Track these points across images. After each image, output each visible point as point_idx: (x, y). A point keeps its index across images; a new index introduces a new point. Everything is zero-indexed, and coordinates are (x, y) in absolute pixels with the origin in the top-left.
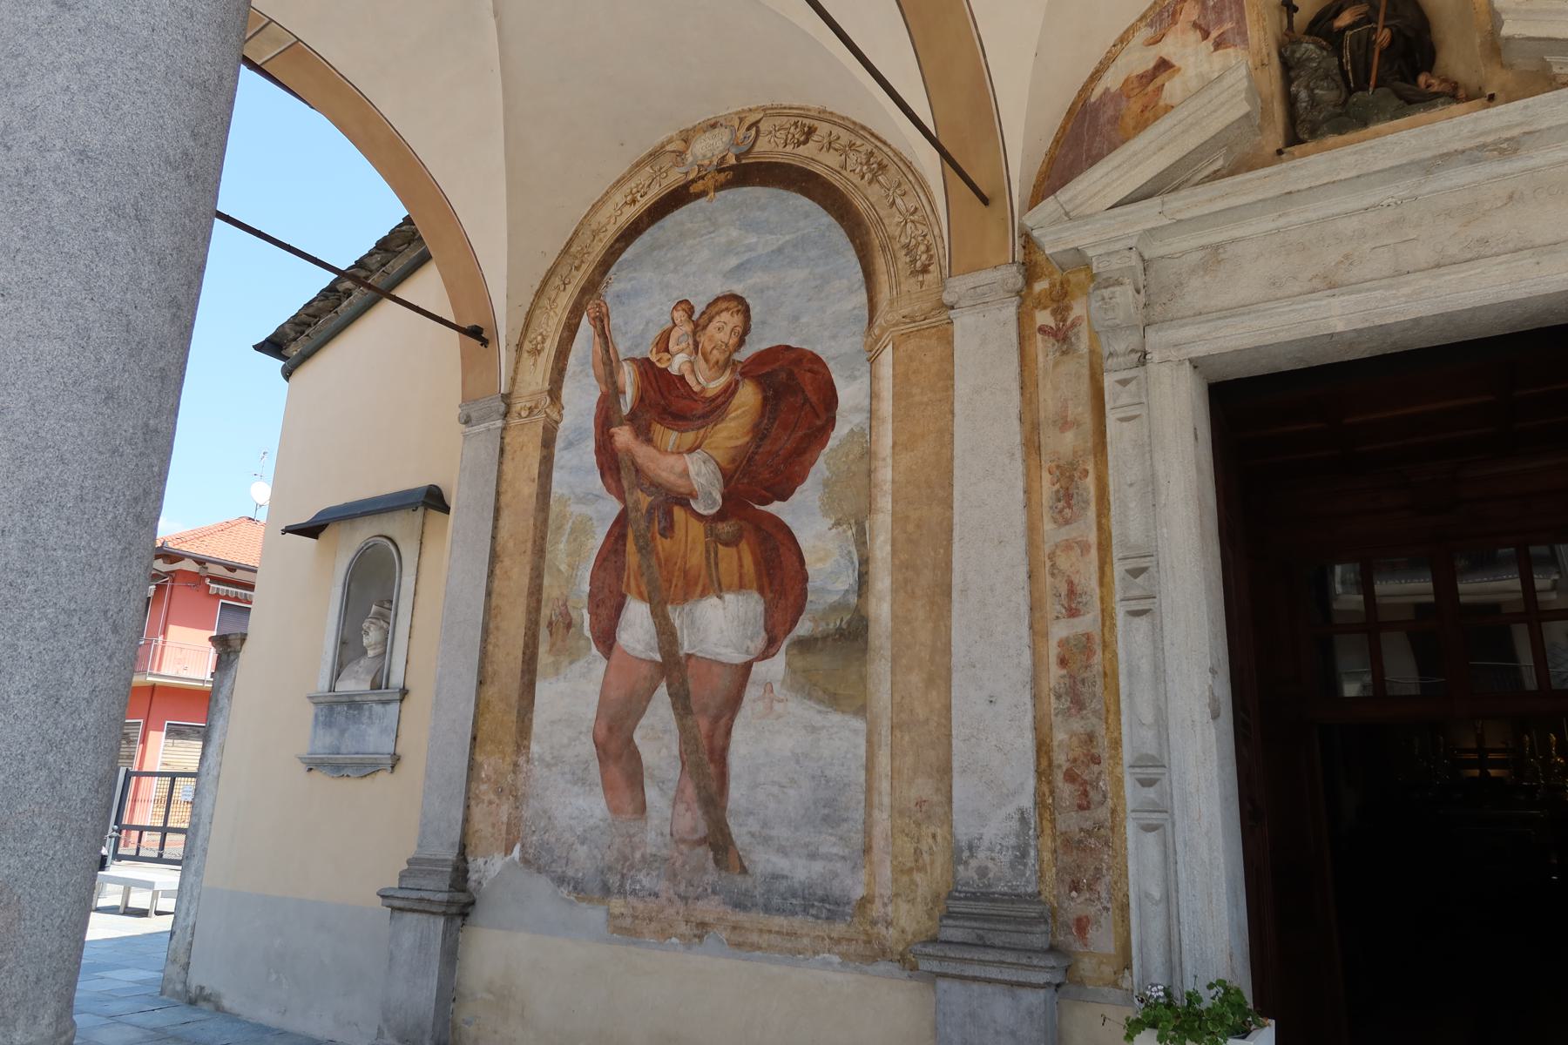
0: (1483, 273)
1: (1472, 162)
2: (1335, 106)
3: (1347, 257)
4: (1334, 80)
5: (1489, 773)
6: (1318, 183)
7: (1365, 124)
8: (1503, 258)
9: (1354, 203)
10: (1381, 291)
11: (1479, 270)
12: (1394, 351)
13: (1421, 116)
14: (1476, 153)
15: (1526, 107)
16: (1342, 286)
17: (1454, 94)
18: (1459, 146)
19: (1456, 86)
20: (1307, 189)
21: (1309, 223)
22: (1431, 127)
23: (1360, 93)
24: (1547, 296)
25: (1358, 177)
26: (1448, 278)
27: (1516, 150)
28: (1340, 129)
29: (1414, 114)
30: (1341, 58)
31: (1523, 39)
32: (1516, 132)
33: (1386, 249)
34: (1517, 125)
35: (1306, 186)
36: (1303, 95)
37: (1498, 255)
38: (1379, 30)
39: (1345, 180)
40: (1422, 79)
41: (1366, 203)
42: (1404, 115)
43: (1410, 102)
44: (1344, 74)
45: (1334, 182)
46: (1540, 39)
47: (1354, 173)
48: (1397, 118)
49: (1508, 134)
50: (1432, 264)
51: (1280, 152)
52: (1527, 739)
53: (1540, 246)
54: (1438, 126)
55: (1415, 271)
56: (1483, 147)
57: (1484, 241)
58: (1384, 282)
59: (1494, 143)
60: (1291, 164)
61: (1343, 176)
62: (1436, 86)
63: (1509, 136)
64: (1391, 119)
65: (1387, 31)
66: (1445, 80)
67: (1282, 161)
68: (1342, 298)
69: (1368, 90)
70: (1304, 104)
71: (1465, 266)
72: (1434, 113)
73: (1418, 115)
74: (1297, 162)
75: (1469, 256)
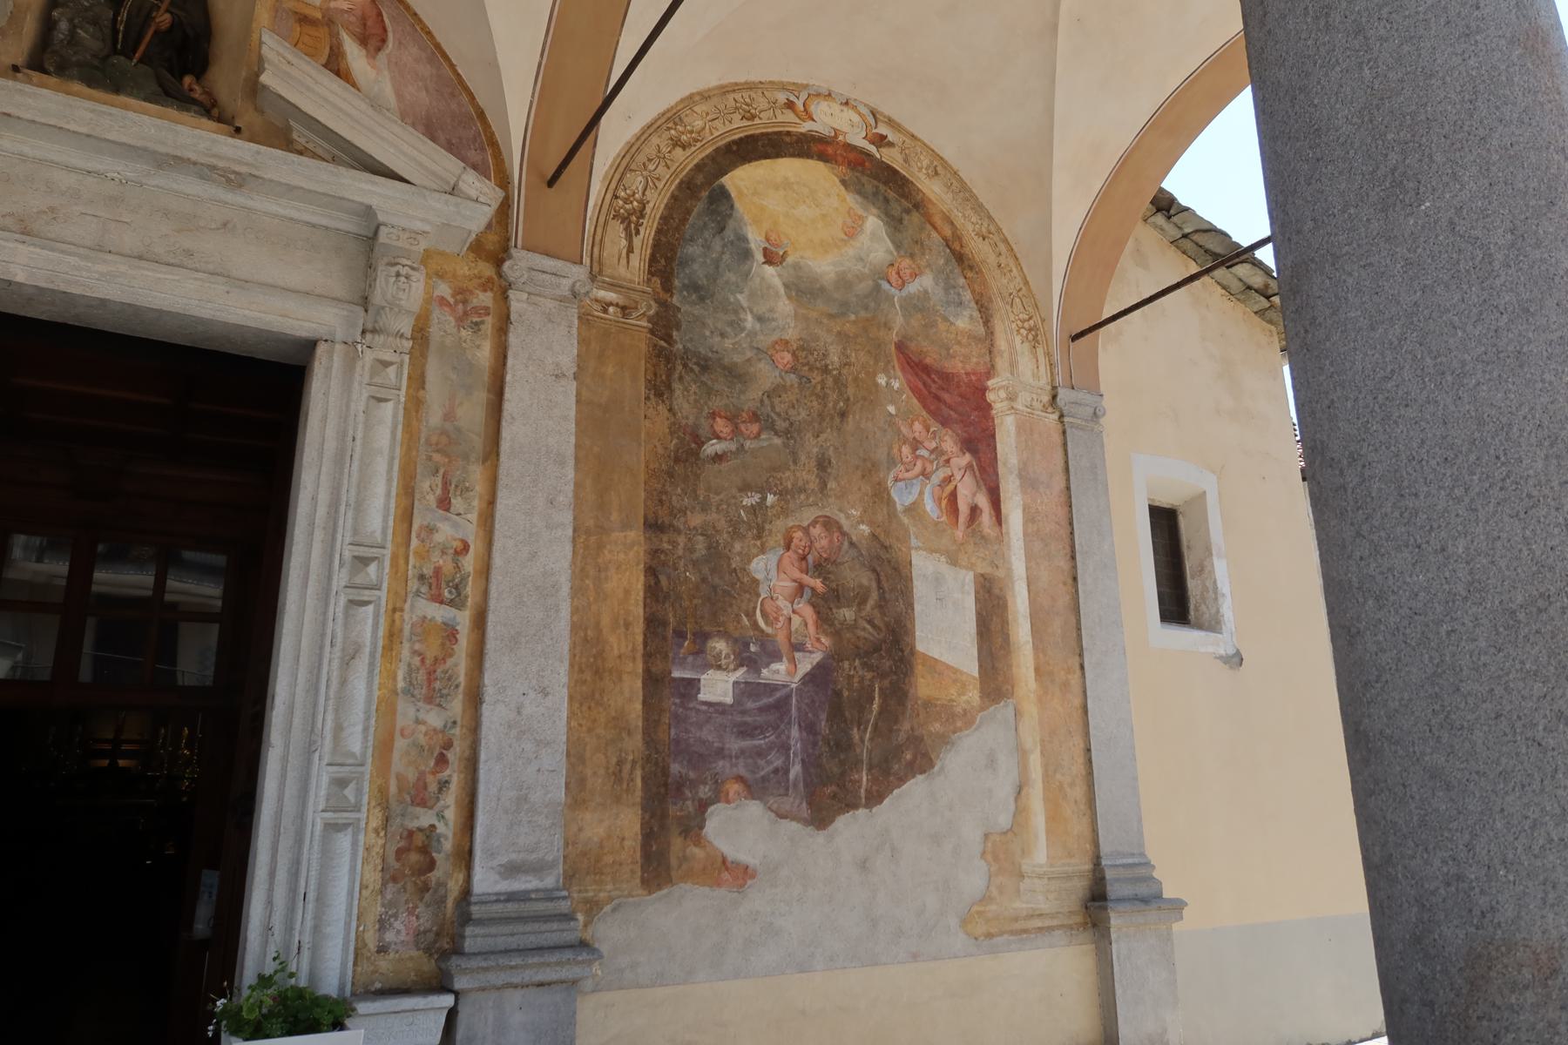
0: (178, 281)
1: (202, 178)
2: (94, 56)
3: (52, 209)
4: (101, 30)
5: (117, 763)
6: (43, 120)
7: (117, 89)
8: (200, 275)
9: (77, 159)
10: (76, 259)
11: (177, 278)
12: (76, 324)
13: (172, 112)
14: (206, 170)
15: (258, 153)
16: (36, 236)
17: (210, 109)
18: (193, 157)
19: (215, 104)
20: (28, 121)
21: (23, 158)
22: (173, 126)
23: (122, 58)
24: (226, 324)
25: (88, 136)
26: (146, 273)
27: (241, 186)
28: (91, 82)
29: (166, 106)
30: (116, 14)
31: (275, 94)
32: (244, 169)
33: (95, 220)
34: (247, 164)
35: (28, 116)
36: (64, 26)
37: (197, 270)
38: (162, 11)
39: (74, 132)
40: (188, 80)
41: (90, 166)
42: (156, 102)
43: (167, 94)
44: (115, 32)
45: (61, 128)
46: (289, 102)
47: (84, 130)
48: (150, 102)
49: (237, 168)
50: (136, 254)
51: (16, 69)
52: (163, 731)
53: (234, 278)
54: (179, 127)
55: (117, 254)
56: (213, 168)
57: (189, 253)
58: (81, 251)
59: (222, 169)
60: (19, 86)
61: (73, 127)
62: (198, 94)
63: (236, 169)
64: (145, 100)
65: (167, 16)
66: (209, 94)
67: (15, 79)
68: (31, 249)
69: (131, 59)
70: (61, 36)
71: (164, 268)
72: (185, 116)
73: (170, 110)
74: (28, 88)
75: (172, 261)
